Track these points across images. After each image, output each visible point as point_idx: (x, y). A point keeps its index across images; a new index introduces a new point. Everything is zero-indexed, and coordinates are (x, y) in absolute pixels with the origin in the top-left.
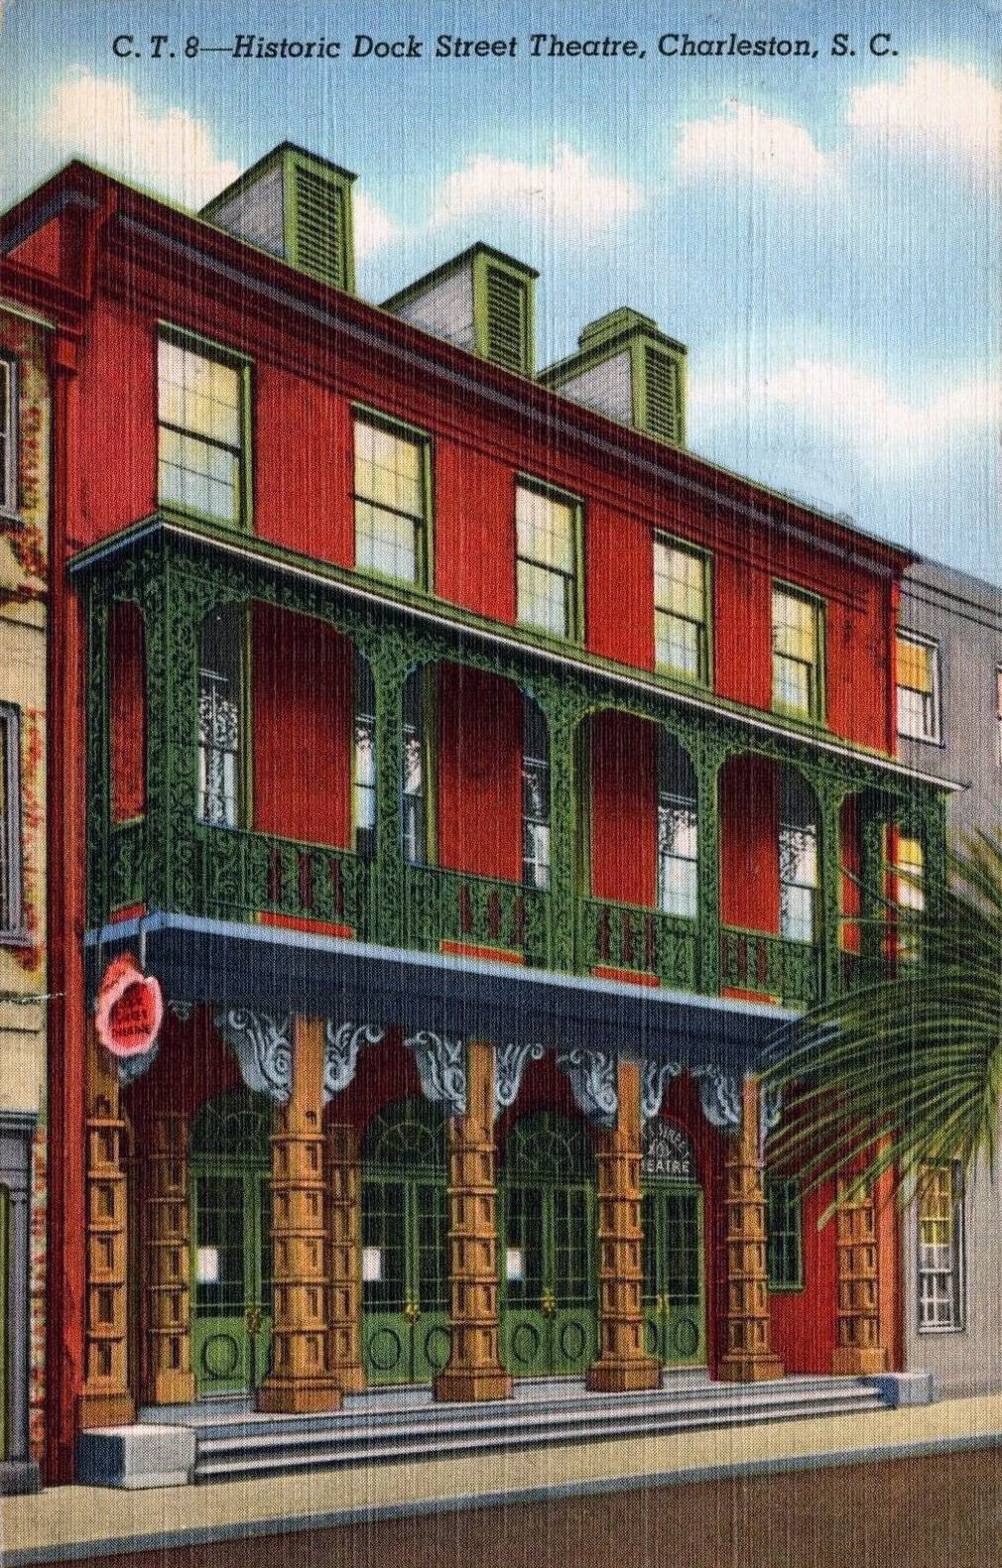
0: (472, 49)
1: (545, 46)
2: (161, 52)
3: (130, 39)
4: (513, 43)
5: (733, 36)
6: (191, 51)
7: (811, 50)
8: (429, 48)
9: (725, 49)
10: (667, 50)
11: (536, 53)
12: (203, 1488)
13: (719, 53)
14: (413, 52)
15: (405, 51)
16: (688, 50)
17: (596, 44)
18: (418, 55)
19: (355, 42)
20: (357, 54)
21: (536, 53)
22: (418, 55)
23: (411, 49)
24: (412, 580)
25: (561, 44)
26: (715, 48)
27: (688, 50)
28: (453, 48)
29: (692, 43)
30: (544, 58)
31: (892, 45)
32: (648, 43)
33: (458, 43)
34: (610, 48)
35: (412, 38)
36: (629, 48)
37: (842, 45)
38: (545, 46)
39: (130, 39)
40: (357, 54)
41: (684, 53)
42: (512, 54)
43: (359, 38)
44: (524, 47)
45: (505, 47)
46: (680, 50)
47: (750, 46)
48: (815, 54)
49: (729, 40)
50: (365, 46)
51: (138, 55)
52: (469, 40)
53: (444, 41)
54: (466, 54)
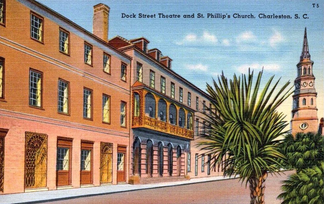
0: (177, 16)
1: (161, 16)
2: (161, 16)
3: (306, 15)
4: (155, 15)
5: (274, 14)
6: (185, 16)
7: (254, 17)
8: (196, 16)
9: (273, 17)
10: (260, 17)
11: (160, 17)
12: (309, 44)
13: (271, 18)
14: (134, 16)
15: (133, 16)
16: (212, 17)
17: (172, 16)
18: (135, 17)
19: (122, 15)
20: (122, 17)
21: (160, 17)
22: (135, 17)
23: (134, 16)
24: (149, 49)
25: (266, 16)
26: (270, 17)
27: (212, 17)
28: (142, 16)
29: (164, 15)
30: (161, 18)
31: (307, 16)
32: (256, 15)
33: (143, 15)
34: (175, 16)
35: (133, 14)
36: (289, 17)
37: (296, 16)
38: (161, 16)
39: (306, 15)
40: (122, 17)
41: (238, 17)
42: (155, 17)
43: (123, 14)
44: (182, 17)
45: (153, 16)
46: (238, 17)
47: (277, 16)
48: (291, 18)
49: (273, 15)
50: (124, 16)
51: (308, 18)
52: (146, 15)
53: (140, 15)
54: (176, 17)
